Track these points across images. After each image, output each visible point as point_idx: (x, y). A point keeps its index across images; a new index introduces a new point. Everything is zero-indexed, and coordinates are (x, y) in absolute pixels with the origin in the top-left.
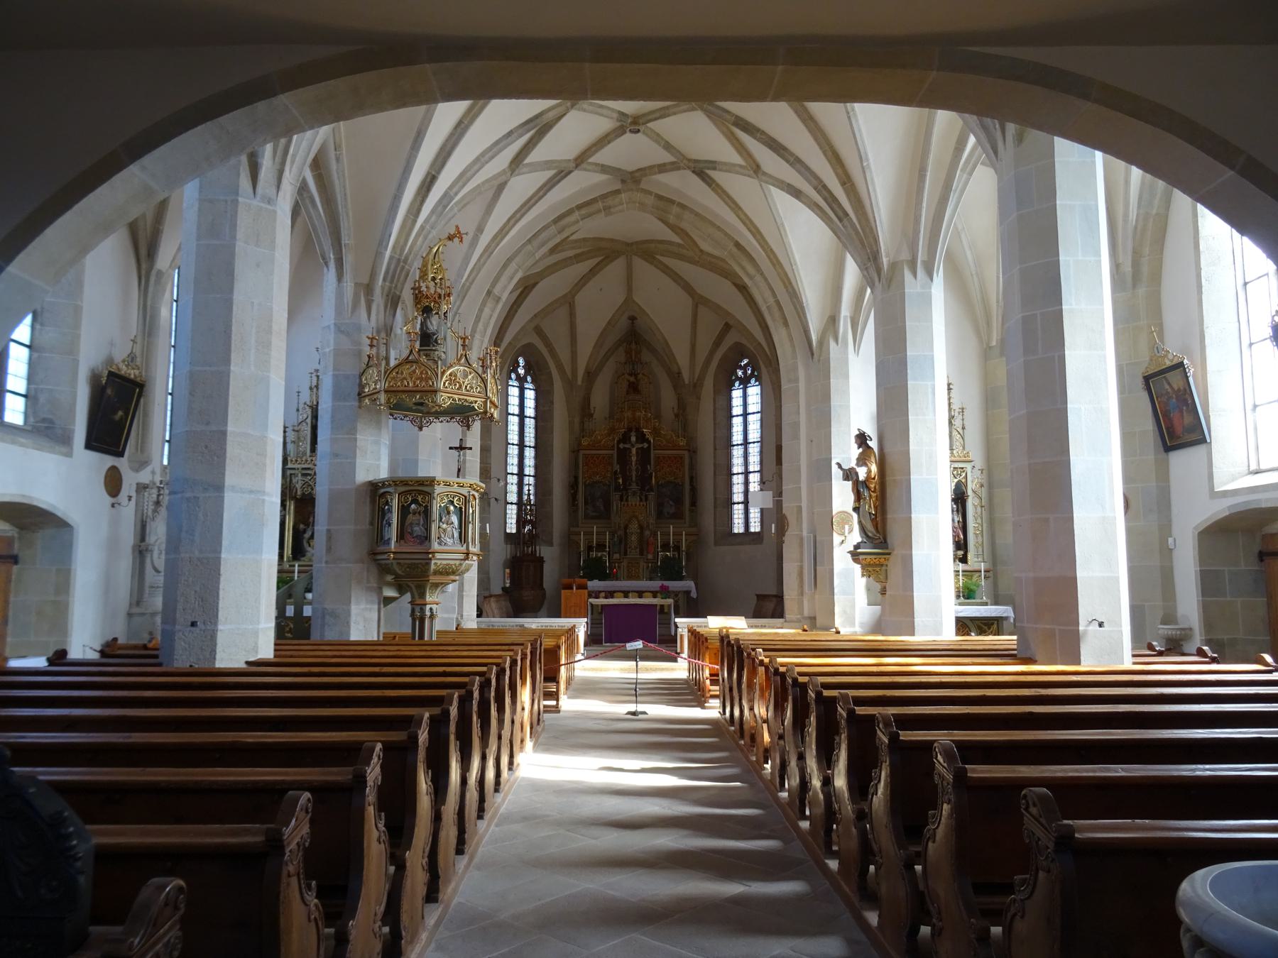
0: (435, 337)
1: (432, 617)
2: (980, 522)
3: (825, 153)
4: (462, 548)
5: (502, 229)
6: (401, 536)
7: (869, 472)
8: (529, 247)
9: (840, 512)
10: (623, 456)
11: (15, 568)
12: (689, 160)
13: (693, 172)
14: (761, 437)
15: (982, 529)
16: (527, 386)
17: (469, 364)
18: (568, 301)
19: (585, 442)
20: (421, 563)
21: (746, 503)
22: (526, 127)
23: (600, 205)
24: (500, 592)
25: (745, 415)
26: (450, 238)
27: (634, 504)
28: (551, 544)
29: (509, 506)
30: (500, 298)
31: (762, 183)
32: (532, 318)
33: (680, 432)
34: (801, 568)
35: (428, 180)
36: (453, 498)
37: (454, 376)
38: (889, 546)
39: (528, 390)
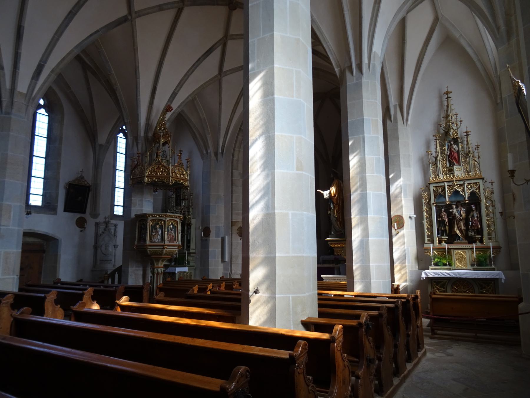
7: (330, 193)
11: (44, 255)
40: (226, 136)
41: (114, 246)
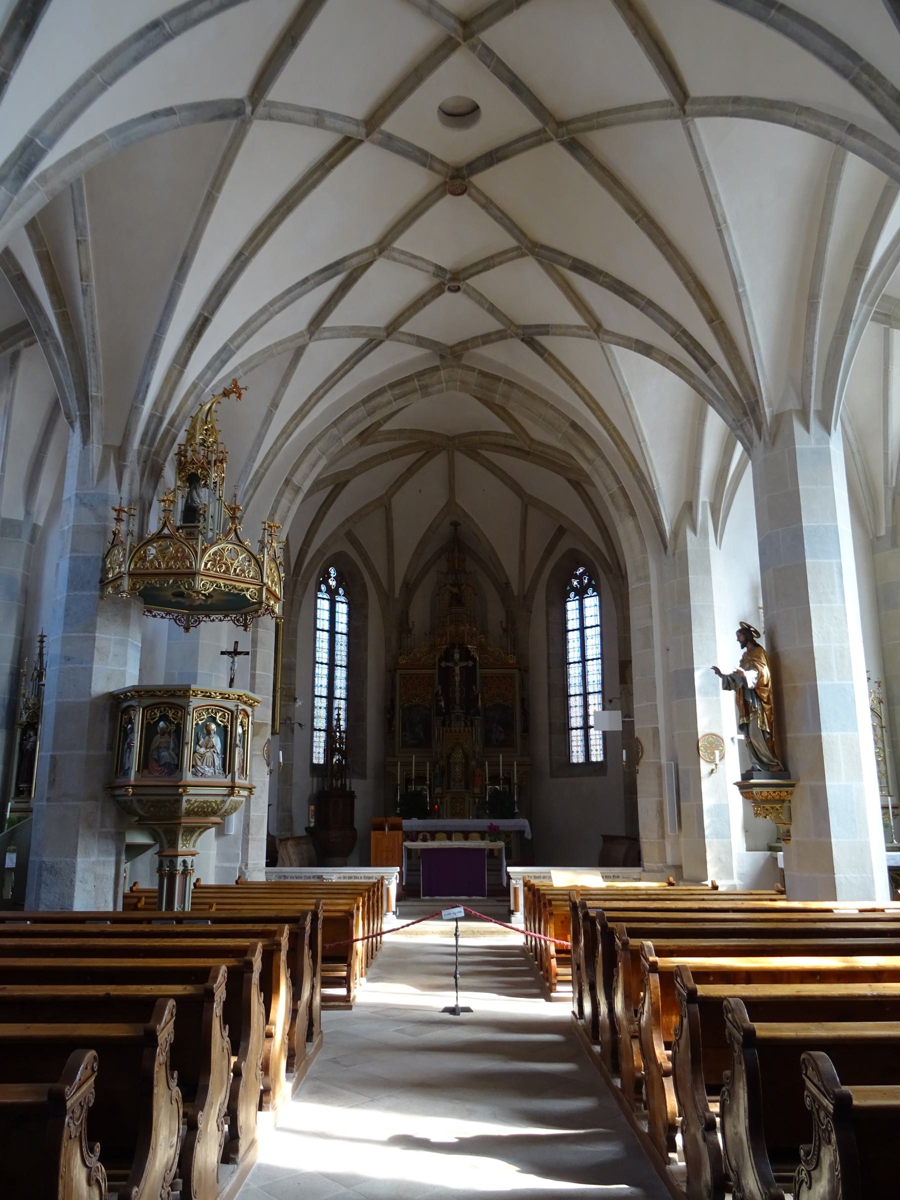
1: (186, 873)
2: (882, 747)
3: (687, 286)
5: (301, 409)
6: (144, 764)
7: (760, 676)
8: (334, 431)
9: (709, 734)
10: (446, 675)
12: (518, 327)
13: (523, 340)
14: (602, 654)
15: (884, 754)
16: (338, 598)
17: (240, 542)
18: (384, 504)
19: (403, 661)
20: (169, 801)
21: (586, 728)
22: (322, 275)
23: (416, 383)
24: (304, 833)
25: (582, 629)
26: (226, 394)
27: (457, 730)
28: (363, 776)
29: (316, 733)
31: (603, 344)
32: (344, 522)
33: (509, 648)
34: (661, 805)
35: (200, 323)
36: (216, 714)
37: (219, 556)
38: (792, 774)
39: (340, 604)
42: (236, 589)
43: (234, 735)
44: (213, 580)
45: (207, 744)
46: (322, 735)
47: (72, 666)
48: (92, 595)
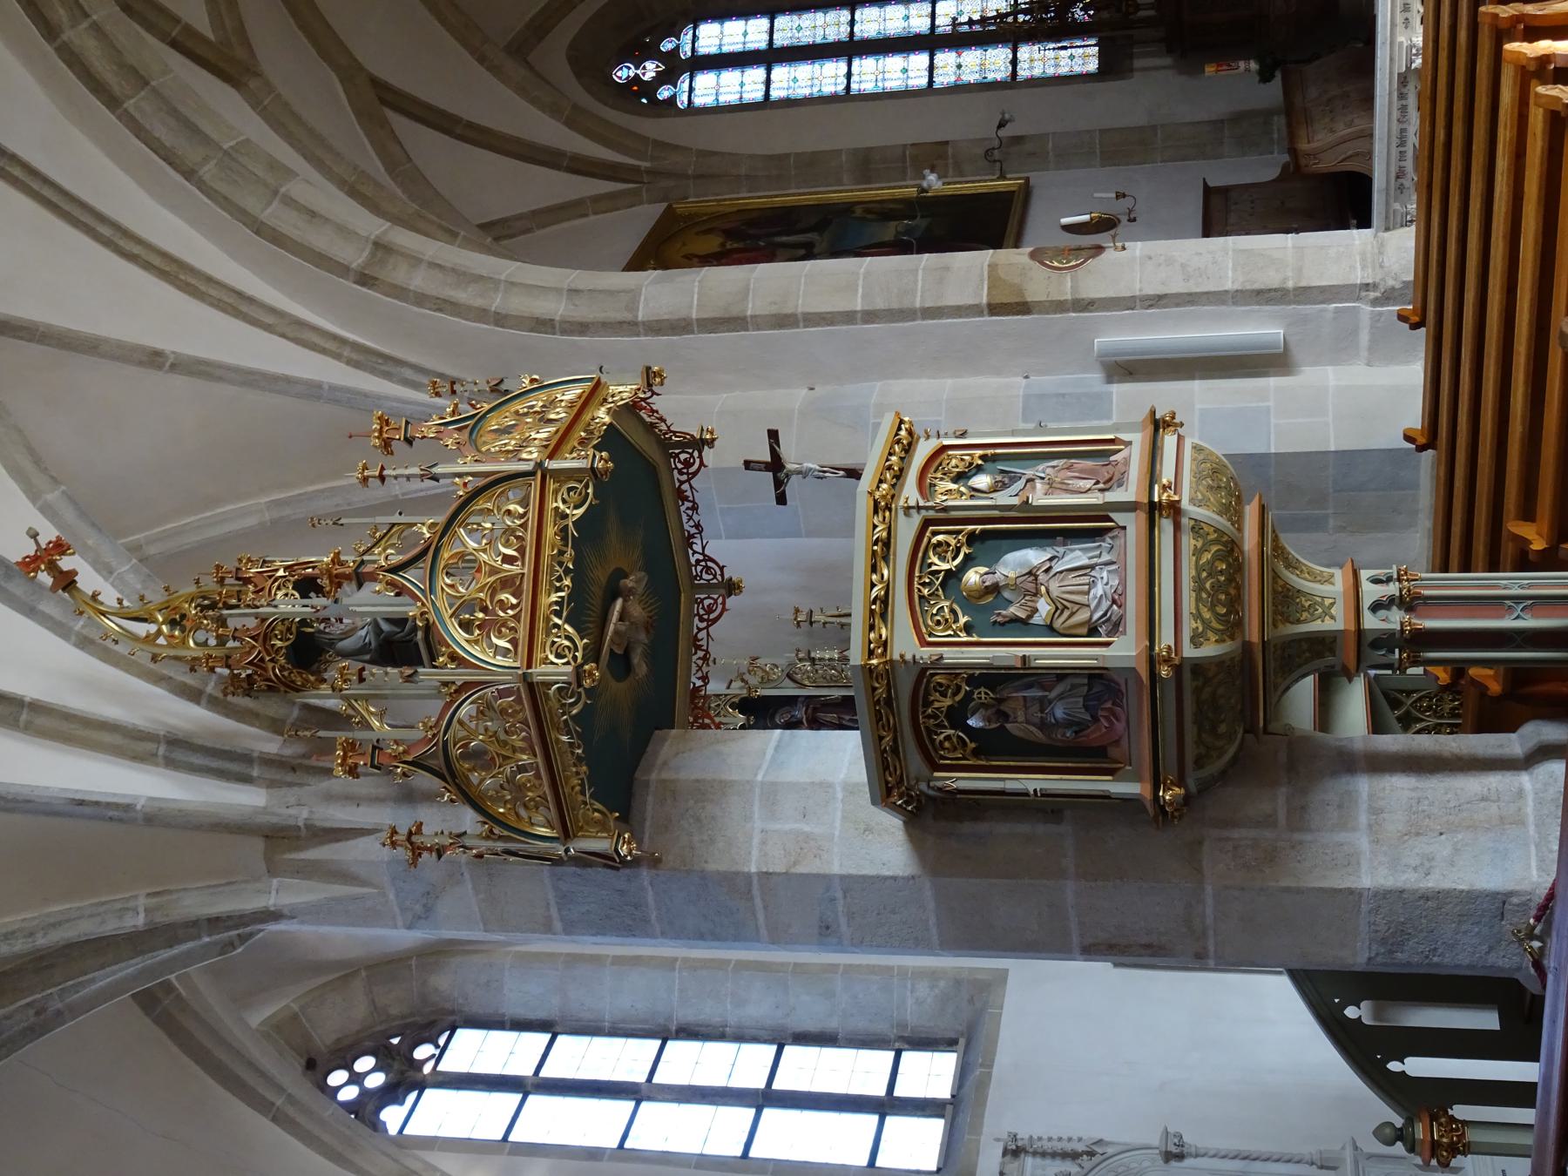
0: (385, 627)
4: (1131, 531)
5: (163, 274)
6: (1097, 758)
8: (208, 171)
17: (424, 552)
20: (1197, 691)
24: (1276, 85)
30: (377, 245)
40: (408, 374)
41: (1174, 1163)
42: (561, 553)
43: (996, 513)
44: (541, 625)
45: (1026, 593)
46: (1027, 55)
47: (843, 920)
48: (651, 884)
